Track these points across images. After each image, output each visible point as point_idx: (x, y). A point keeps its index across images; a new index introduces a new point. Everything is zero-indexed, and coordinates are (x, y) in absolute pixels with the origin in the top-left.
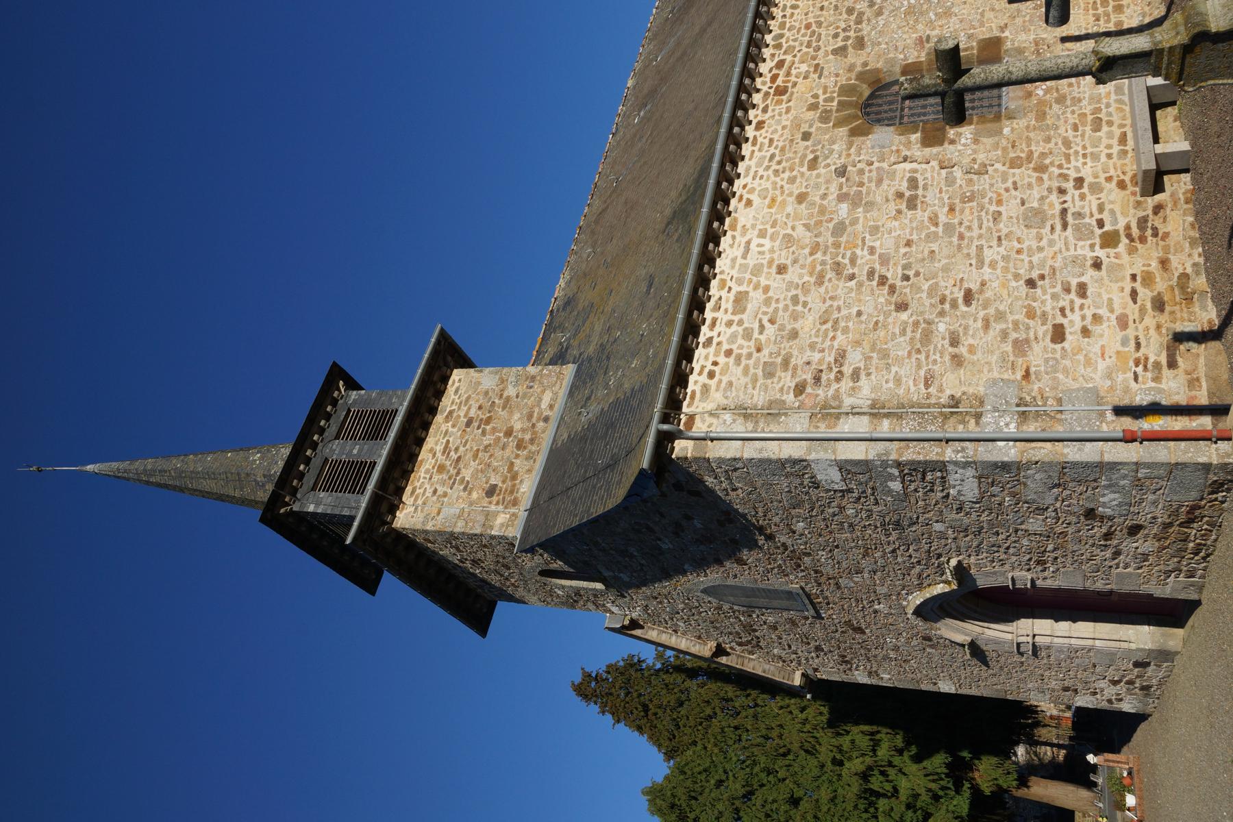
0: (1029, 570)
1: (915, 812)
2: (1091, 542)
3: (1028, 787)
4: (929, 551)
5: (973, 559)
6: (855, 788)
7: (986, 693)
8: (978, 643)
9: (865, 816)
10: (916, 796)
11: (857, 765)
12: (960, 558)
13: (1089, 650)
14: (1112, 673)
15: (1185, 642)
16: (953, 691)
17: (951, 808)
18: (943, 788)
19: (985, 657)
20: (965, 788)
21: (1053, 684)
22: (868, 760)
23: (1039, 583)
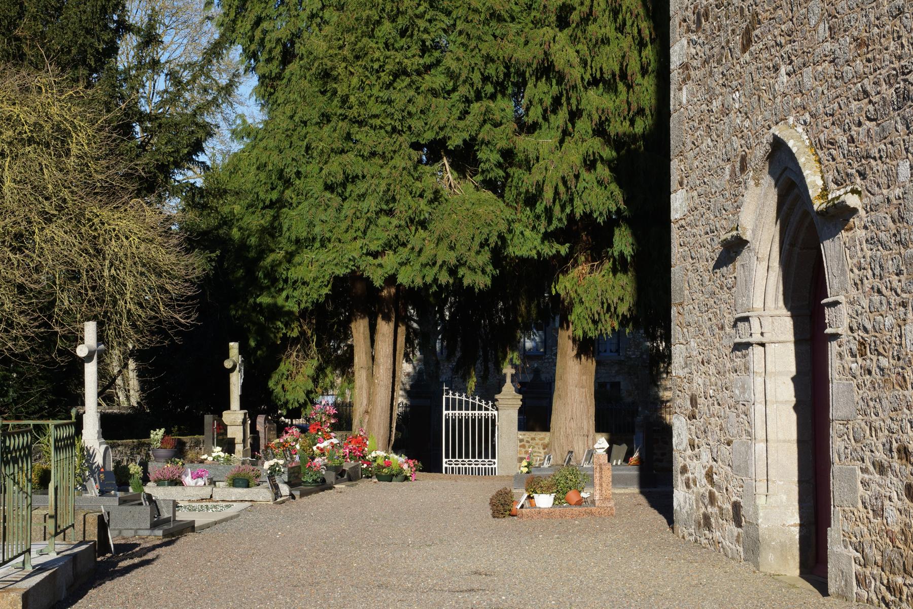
0: (851, 329)
1: (499, 165)
2: (895, 427)
3: (578, 356)
4: (868, 157)
5: (861, 234)
6: (524, 55)
7: (676, 272)
8: (745, 253)
9: (476, 77)
10: (527, 166)
11: (565, 54)
12: (862, 212)
13: (749, 434)
14: (722, 471)
15: (774, 577)
16: (674, 215)
17: (518, 228)
18: (549, 212)
19: (726, 265)
20: (556, 246)
21: (699, 380)
22: (576, 74)
23: (833, 347)
